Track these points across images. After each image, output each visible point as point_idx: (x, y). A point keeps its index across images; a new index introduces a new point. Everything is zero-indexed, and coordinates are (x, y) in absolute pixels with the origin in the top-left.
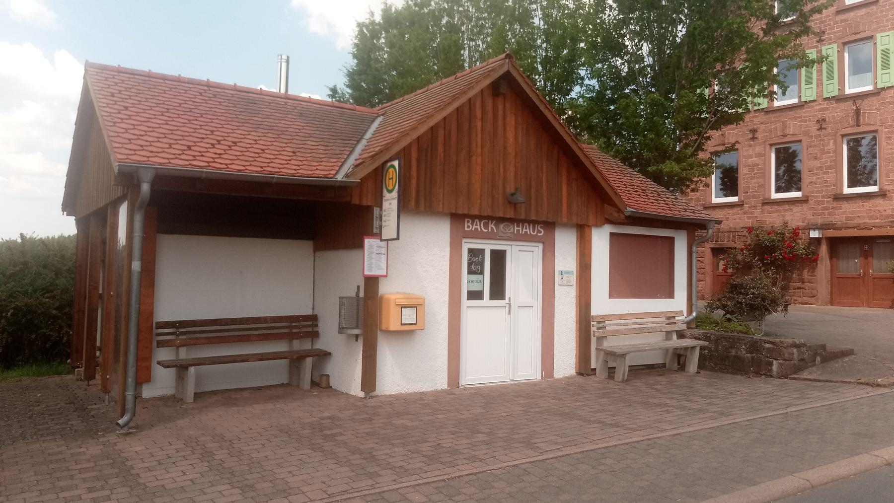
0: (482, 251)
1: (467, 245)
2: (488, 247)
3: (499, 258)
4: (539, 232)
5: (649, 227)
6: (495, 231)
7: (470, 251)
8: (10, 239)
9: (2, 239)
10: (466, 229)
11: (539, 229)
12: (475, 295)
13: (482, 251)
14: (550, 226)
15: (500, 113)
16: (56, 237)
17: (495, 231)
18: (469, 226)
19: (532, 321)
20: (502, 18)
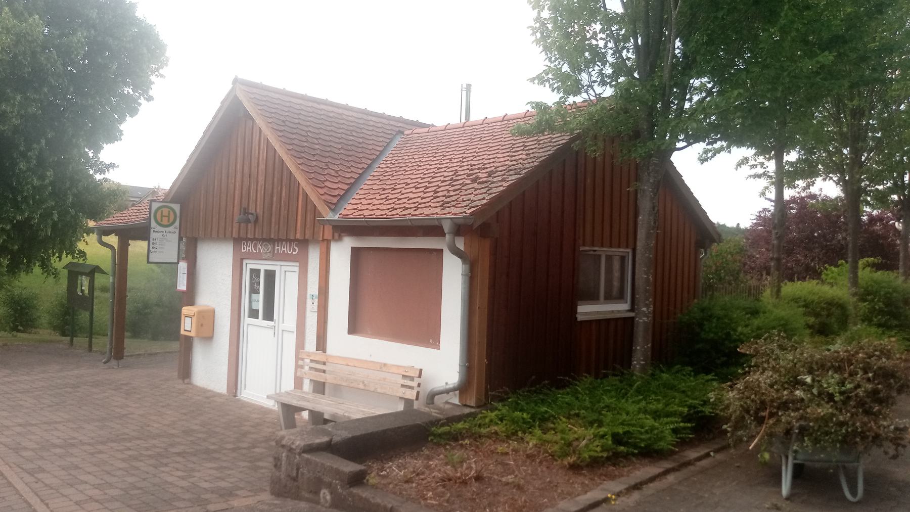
0: (259, 271)
1: (250, 265)
2: (263, 266)
3: (270, 276)
4: (294, 250)
5: (360, 236)
6: (750, 448)
7: (252, 271)
8: (150, 99)
9: (162, 76)
10: (243, 251)
11: (295, 247)
12: (254, 314)
13: (259, 271)
14: (304, 243)
15: (589, 181)
16: (128, 118)
17: (750, 448)
18: (247, 248)
19: (291, 341)
20: (638, 77)
